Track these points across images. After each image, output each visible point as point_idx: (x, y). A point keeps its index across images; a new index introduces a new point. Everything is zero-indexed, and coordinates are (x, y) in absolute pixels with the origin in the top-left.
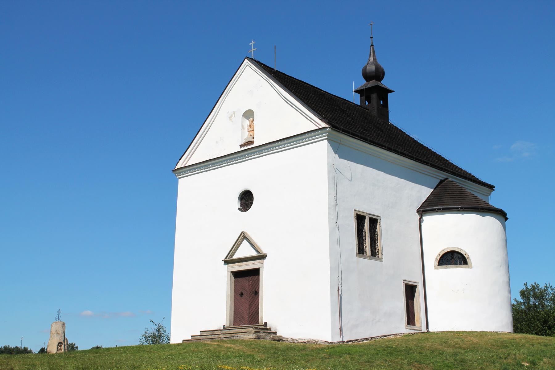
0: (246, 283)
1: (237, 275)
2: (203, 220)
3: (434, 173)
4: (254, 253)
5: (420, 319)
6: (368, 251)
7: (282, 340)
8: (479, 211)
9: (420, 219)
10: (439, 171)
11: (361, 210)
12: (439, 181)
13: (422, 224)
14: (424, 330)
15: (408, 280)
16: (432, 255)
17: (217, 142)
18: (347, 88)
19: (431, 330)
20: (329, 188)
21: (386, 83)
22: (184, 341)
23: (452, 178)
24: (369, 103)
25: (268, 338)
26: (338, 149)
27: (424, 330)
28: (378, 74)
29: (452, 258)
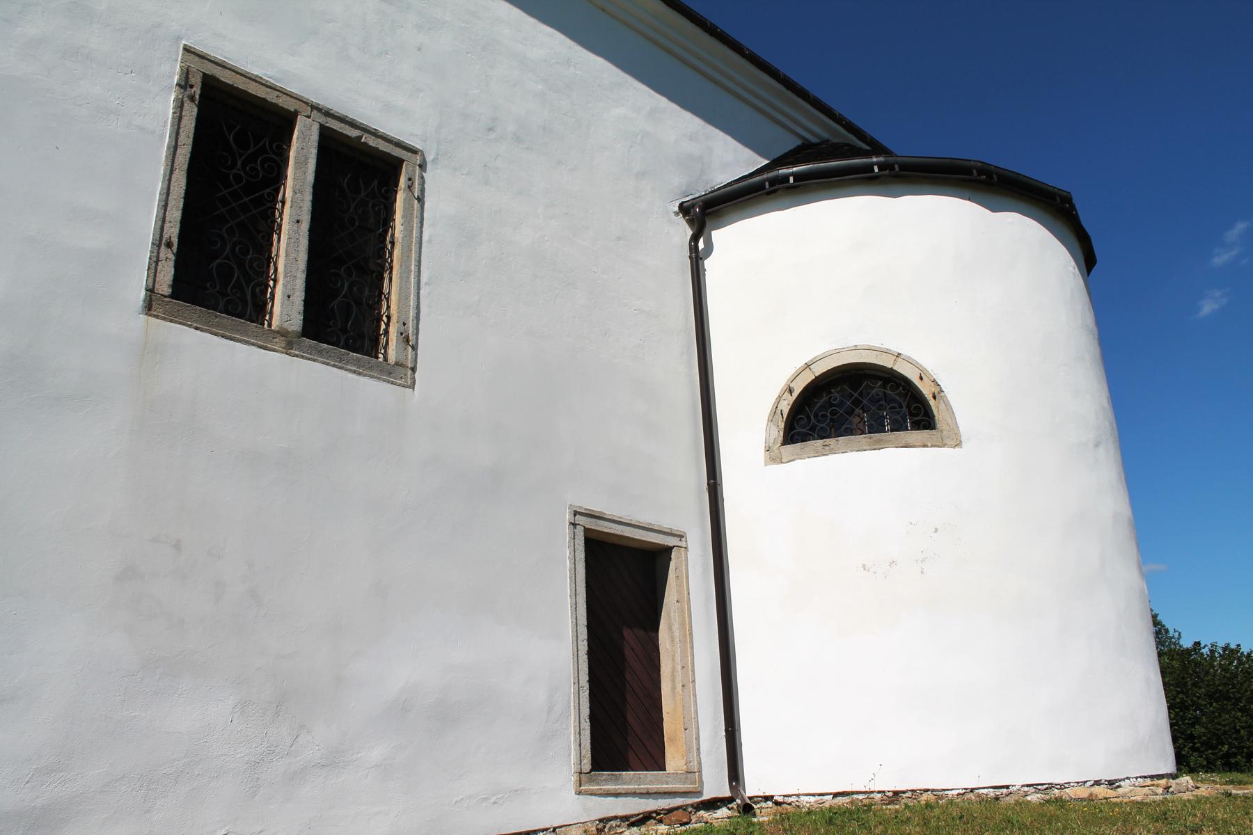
5: (691, 726)
6: (287, 299)
9: (695, 238)
11: (255, 71)
12: (799, 142)
13: (708, 263)
14: (715, 784)
15: (609, 512)
19: (759, 780)
27: (715, 784)
29: (856, 402)
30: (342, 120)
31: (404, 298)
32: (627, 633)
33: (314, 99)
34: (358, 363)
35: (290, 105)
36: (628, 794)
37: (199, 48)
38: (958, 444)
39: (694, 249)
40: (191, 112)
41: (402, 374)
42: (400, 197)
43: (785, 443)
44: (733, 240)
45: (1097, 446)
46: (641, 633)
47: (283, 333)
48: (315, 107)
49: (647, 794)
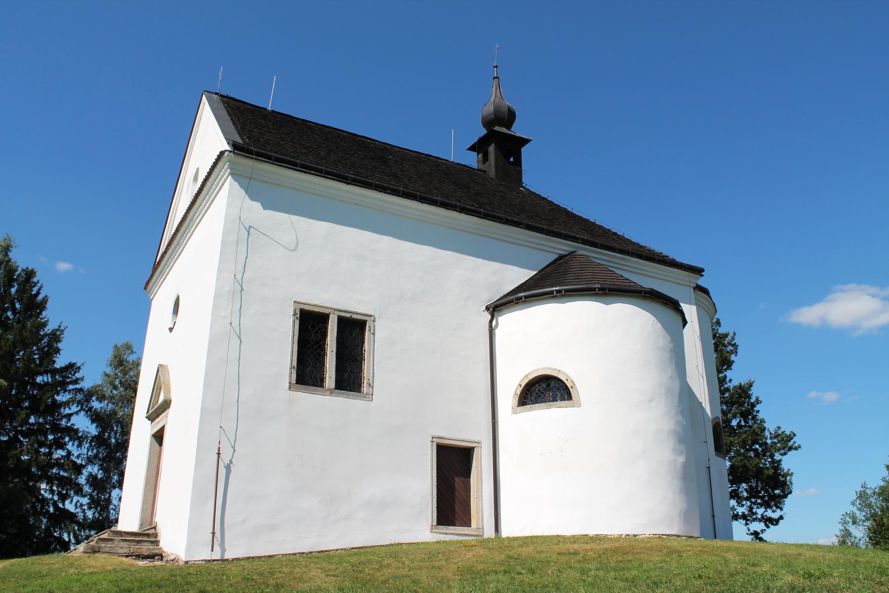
3: (544, 243)
5: (480, 512)
6: (330, 378)
8: (596, 294)
9: (491, 321)
10: (548, 237)
12: (557, 256)
15: (447, 436)
16: (509, 387)
18: (454, 143)
20: (222, 261)
21: (518, 130)
23: (584, 250)
25: (123, 551)
26: (252, 189)
27: (489, 532)
28: (509, 118)
29: (544, 389)
30: (345, 311)
31: (369, 370)
32: (456, 479)
33: (335, 307)
34: (353, 395)
35: (326, 311)
36: (452, 534)
37: (298, 300)
38: (580, 406)
39: (491, 326)
40: (297, 322)
41: (370, 396)
42: (367, 333)
43: (519, 406)
44: (508, 320)
45: (651, 401)
46: (463, 479)
47: (329, 389)
48: (335, 310)
49: (459, 535)
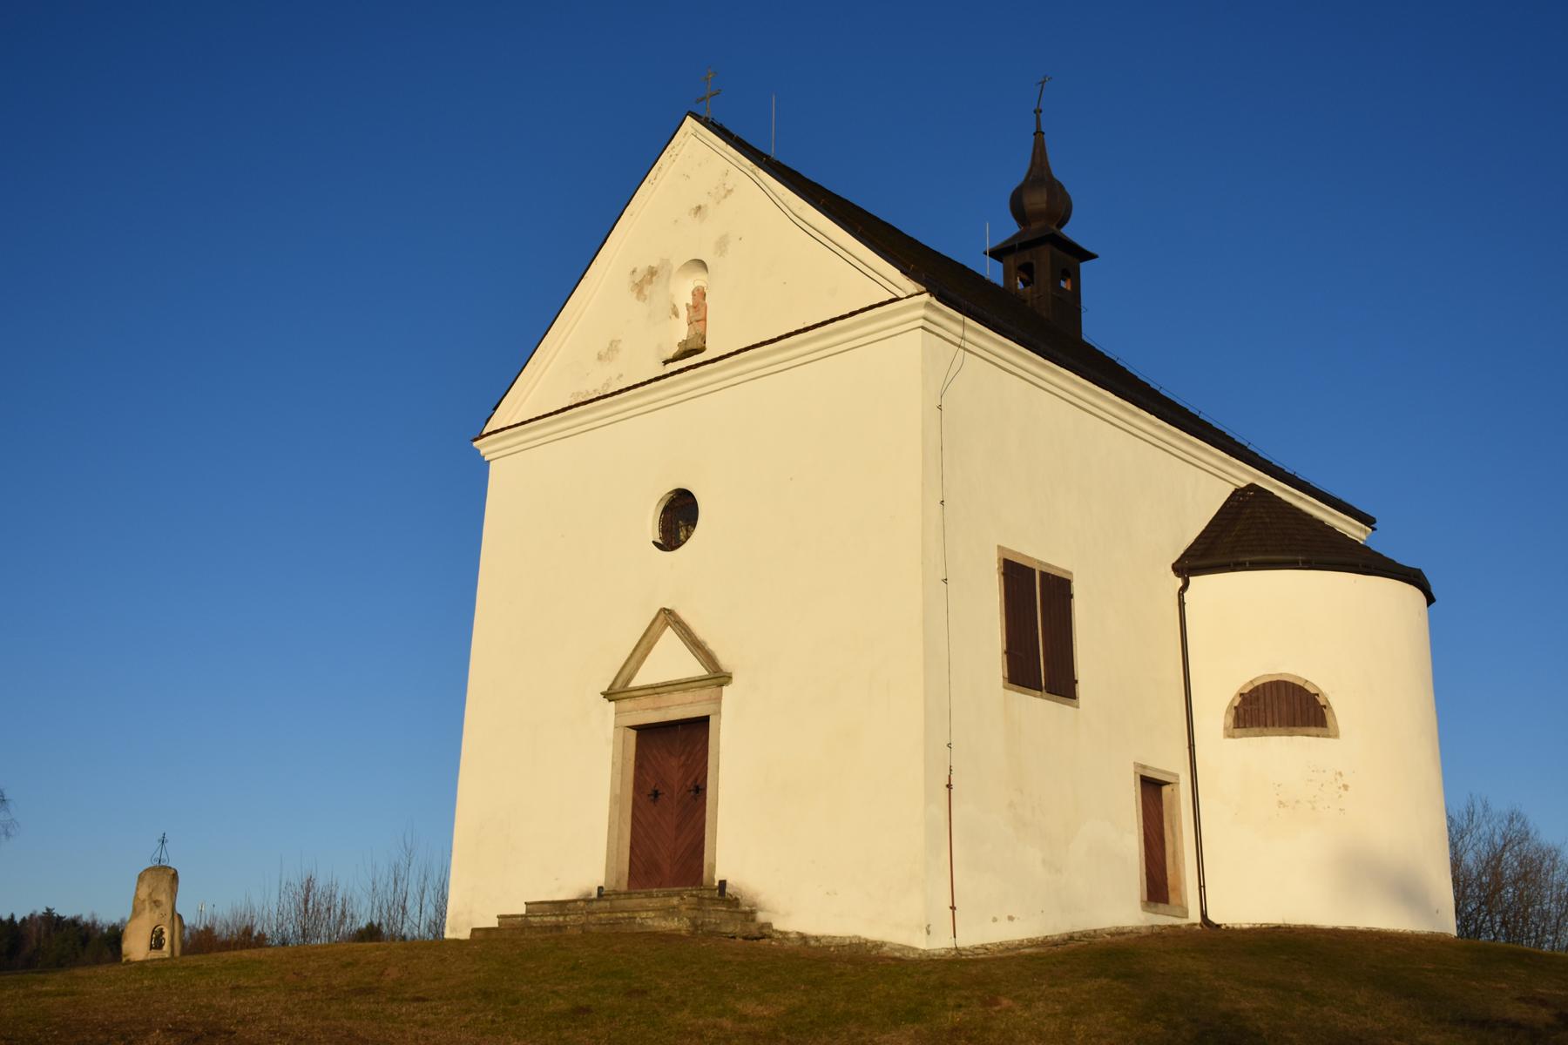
0: (670, 765)
1: (646, 733)
2: (555, 488)
4: (696, 669)
7: (770, 937)
17: (600, 358)
22: (474, 930)
24: (1025, 284)
29: (1282, 707)
